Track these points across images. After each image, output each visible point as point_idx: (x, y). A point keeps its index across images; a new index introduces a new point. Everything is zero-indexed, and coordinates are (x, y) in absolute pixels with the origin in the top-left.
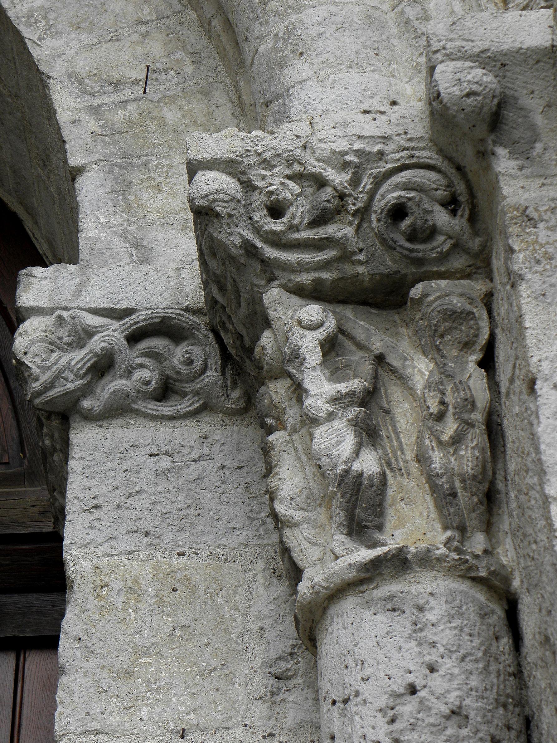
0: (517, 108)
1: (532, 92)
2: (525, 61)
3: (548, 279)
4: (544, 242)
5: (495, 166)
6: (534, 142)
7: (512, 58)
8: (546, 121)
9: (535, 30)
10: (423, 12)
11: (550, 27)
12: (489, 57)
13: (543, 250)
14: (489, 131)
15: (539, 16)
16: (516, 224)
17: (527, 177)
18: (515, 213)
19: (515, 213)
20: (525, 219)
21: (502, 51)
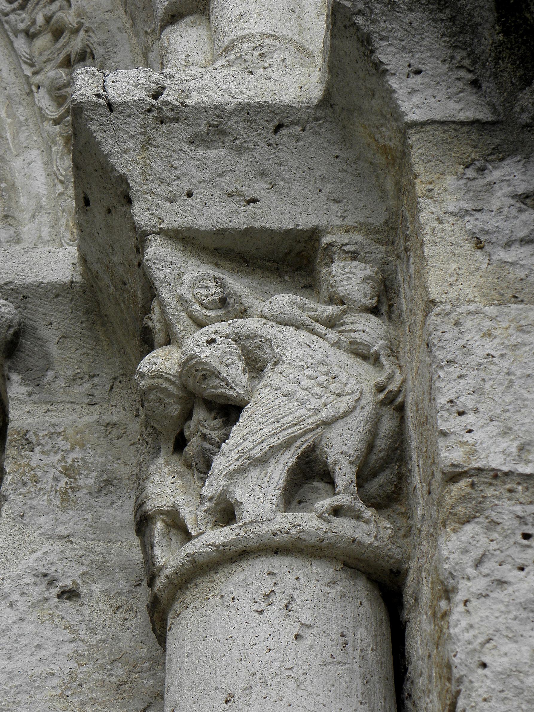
0: (35, 338)
1: (50, 324)
2: (46, 294)
3: (30, 501)
4: (34, 466)
6: (47, 370)
7: (33, 291)
8: (60, 351)
9: (58, 266)
10: (15, 235)
11: (73, 264)
12: (12, 289)
13: (32, 473)
14: (5, 358)
16: (14, 446)
17: (35, 403)
18: (15, 436)
19: (15, 436)
20: (24, 442)
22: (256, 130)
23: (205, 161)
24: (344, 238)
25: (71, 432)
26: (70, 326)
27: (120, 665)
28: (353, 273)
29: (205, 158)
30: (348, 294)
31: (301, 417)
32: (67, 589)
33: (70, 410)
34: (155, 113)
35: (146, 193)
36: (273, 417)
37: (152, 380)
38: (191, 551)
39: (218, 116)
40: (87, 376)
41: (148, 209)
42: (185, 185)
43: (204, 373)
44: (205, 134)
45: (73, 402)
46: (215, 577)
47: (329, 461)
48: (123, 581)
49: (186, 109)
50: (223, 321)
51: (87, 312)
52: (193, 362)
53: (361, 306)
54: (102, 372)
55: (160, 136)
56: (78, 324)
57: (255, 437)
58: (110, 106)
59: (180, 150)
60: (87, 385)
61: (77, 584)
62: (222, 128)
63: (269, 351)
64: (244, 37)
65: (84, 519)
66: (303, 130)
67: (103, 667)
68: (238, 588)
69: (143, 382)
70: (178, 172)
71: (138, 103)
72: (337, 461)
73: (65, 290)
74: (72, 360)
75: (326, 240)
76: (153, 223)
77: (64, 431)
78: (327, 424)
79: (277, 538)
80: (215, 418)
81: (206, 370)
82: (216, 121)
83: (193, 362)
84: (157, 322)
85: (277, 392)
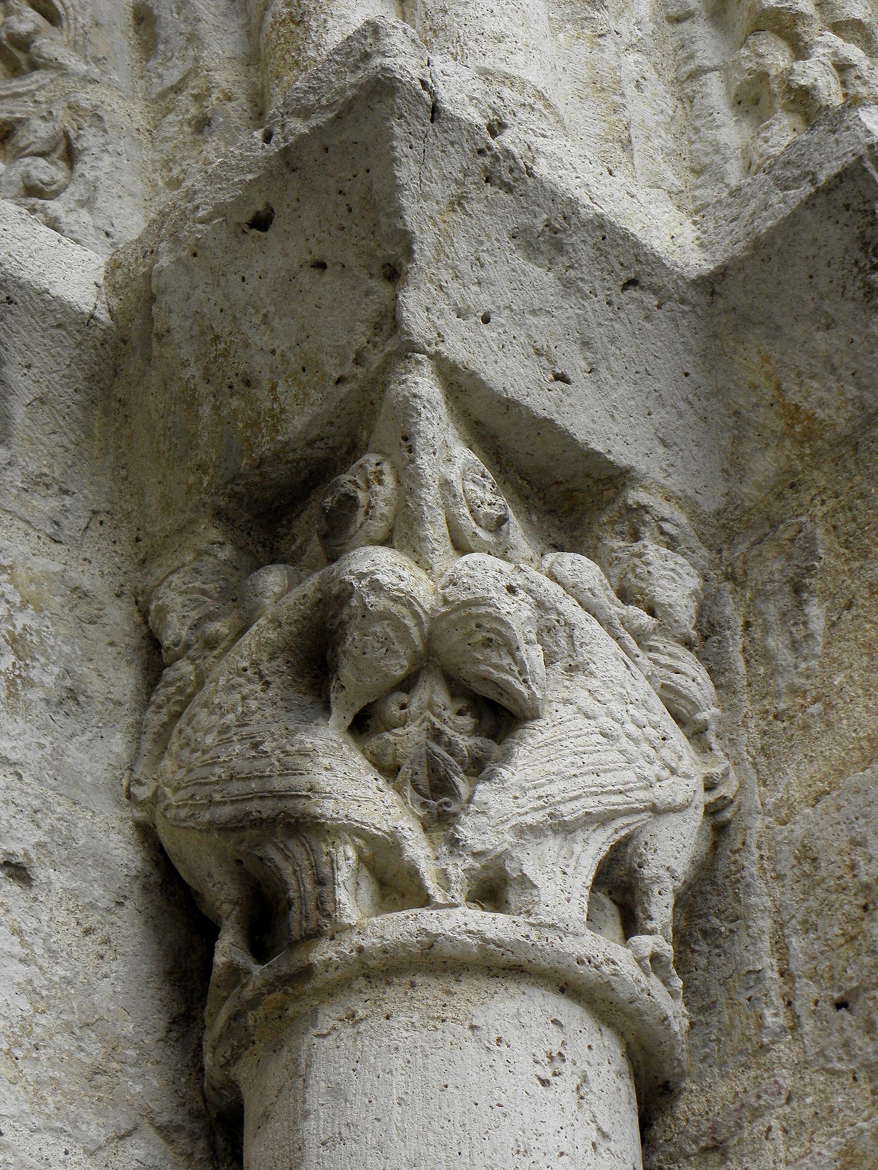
1: (29, 367)
2: (44, 314)
5: (124, 756)
8: (28, 422)
9: (75, 276)
15: (86, 259)
21: (20, 278)
22: (602, 270)
23: (522, 278)
24: (665, 509)
25: (21, 574)
26: (57, 386)
27: (93, 1035)
28: (678, 574)
29: (523, 271)
30: (670, 606)
31: (628, 783)
32: (14, 861)
33: (21, 533)
34: (487, 161)
35: (431, 281)
36: (593, 764)
37: (391, 604)
38: (434, 927)
39: (565, 218)
40: (56, 487)
41: (428, 309)
42: (483, 300)
43: (493, 636)
44: (536, 235)
45: (28, 522)
46: (456, 988)
47: (647, 872)
48: (99, 886)
49: (530, 181)
50: (489, 553)
51: (91, 378)
52: (483, 610)
53: (684, 634)
54: (80, 491)
55: (479, 201)
56: (69, 391)
57: (568, 785)
58: (435, 111)
59: (497, 239)
60: (54, 503)
61: (31, 860)
62: (562, 239)
63: (563, 643)
64: (507, 76)
65: (40, 744)
66: (659, 307)
67: (68, 1027)
68: (507, 1025)
69: (372, 599)
70: (483, 274)
71: (473, 129)
72: (658, 878)
73: (77, 324)
74: (42, 447)
75: (636, 496)
76: (429, 336)
77: (11, 567)
78: (656, 810)
79: (581, 969)
80: (460, 713)
81: (499, 633)
82: (560, 224)
83: (483, 610)
84: (384, 500)
85: (590, 721)
